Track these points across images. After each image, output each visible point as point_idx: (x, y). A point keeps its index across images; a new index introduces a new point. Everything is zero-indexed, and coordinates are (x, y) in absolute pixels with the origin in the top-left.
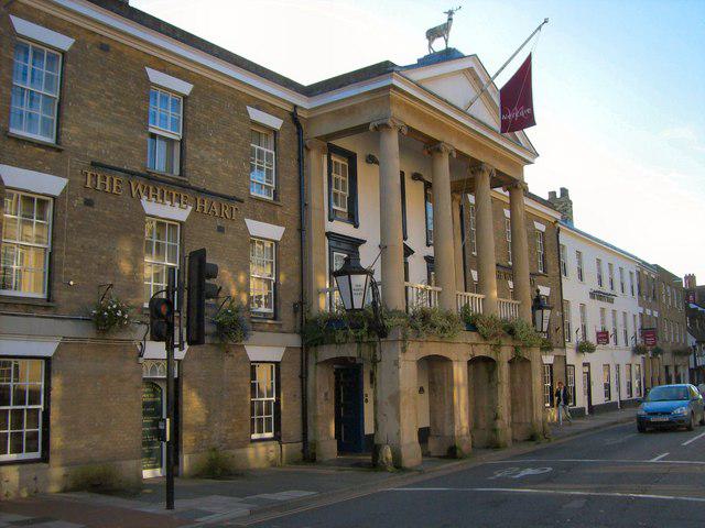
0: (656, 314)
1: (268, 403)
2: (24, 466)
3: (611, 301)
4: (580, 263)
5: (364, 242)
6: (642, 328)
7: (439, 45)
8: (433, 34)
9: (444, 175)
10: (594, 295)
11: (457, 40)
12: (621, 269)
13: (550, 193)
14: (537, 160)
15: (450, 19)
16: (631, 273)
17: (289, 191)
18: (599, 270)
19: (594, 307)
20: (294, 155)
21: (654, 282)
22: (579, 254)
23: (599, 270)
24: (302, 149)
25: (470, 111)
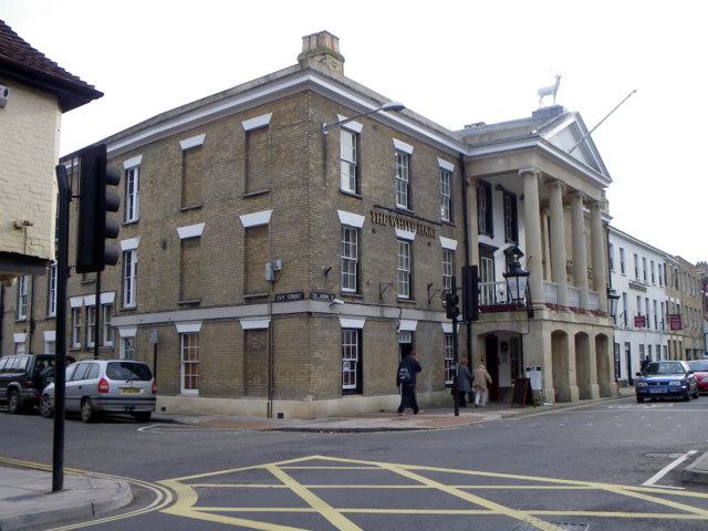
0: (678, 302)
1: (352, 362)
2: (67, 456)
3: (644, 290)
4: (622, 258)
5: (99, 95)
6: (667, 314)
7: (548, 102)
8: (543, 93)
9: (558, 197)
10: (632, 286)
11: (567, 100)
12: (644, 259)
13: (307, 39)
14: (611, 185)
15: (558, 83)
16: (660, 266)
17: (458, 220)
18: (636, 263)
19: (632, 295)
20: (460, 189)
21: (676, 271)
22: (621, 250)
23: (636, 263)
24: (465, 185)
25: (572, 154)
